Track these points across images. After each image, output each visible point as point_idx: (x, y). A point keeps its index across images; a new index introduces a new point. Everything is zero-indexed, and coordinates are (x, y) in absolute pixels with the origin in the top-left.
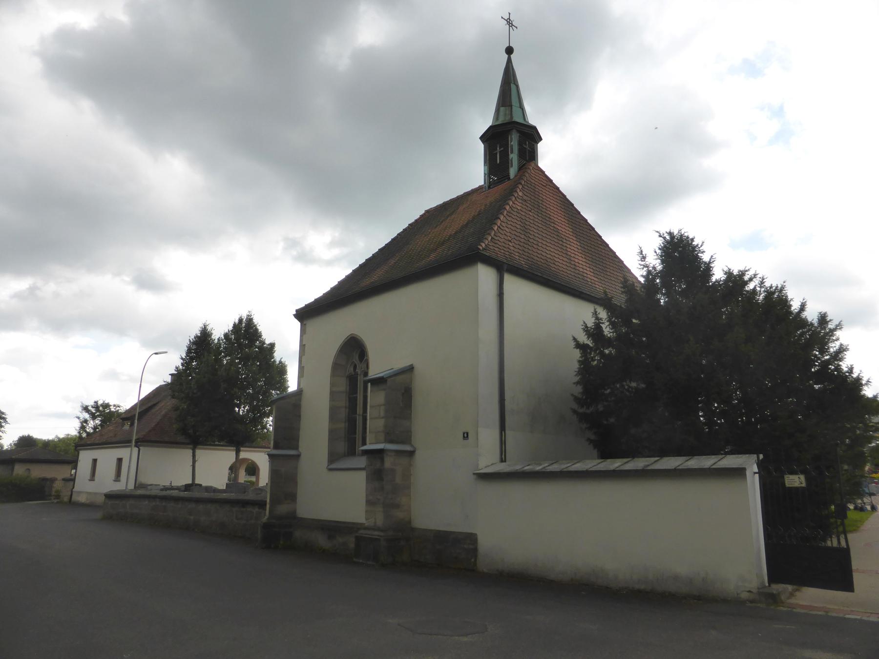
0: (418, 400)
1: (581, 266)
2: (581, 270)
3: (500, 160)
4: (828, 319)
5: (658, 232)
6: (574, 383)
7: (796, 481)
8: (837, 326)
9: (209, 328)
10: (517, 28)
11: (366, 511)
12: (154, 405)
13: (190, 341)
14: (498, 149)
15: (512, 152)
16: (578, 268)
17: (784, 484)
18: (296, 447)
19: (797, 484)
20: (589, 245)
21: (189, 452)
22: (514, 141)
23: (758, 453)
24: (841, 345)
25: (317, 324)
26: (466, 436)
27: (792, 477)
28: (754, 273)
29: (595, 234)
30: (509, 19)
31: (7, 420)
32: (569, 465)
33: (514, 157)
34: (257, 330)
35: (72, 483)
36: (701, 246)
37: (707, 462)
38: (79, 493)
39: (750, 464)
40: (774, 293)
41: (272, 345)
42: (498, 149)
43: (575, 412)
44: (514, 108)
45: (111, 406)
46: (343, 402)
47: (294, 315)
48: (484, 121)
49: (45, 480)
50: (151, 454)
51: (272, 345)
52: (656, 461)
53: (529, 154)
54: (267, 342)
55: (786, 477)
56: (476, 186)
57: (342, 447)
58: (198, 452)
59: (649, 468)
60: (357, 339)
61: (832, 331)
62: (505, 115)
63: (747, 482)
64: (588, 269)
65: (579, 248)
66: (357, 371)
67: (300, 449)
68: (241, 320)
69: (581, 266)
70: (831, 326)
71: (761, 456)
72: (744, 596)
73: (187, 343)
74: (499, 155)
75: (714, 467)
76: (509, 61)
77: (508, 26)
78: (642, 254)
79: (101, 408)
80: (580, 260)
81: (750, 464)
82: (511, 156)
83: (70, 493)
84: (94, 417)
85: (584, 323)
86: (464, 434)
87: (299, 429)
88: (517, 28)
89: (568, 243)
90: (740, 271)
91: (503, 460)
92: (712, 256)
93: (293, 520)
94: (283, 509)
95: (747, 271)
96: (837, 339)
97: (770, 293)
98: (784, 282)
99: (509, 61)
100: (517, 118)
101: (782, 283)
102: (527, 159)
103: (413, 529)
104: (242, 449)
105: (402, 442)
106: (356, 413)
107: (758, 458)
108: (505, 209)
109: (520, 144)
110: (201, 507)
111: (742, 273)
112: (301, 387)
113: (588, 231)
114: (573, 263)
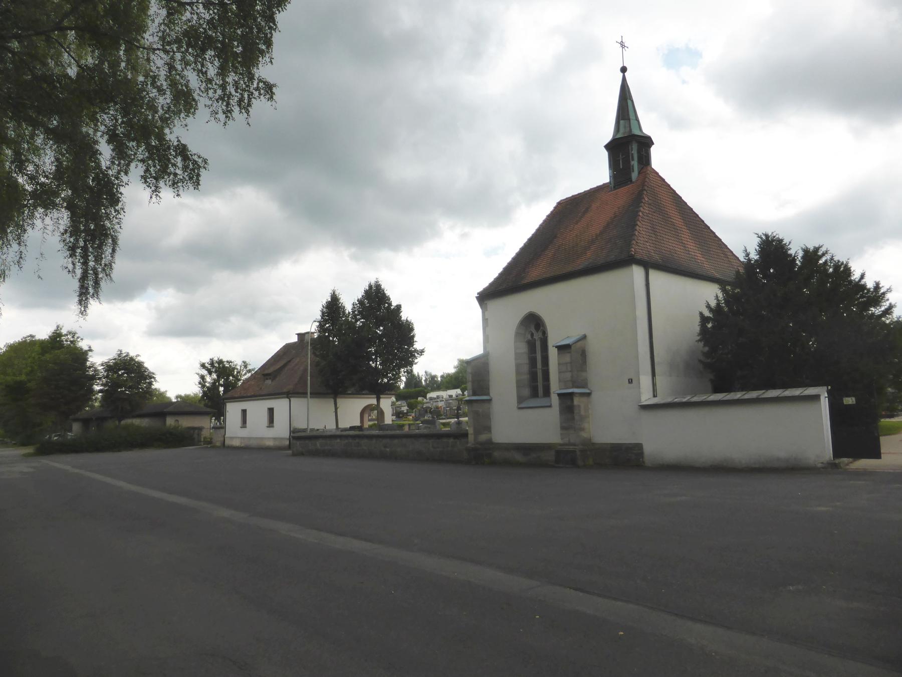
0: (592, 359)
1: (692, 250)
2: (693, 254)
3: (622, 165)
4: (881, 286)
5: (756, 234)
6: (696, 341)
7: (849, 401)
8: (888, 289)
9: (337, 293)
10: (628, 47)
11: (561, 434)
12: (289, 361)
13: (323, 306)
14: (621, 156)
15: (633, 160)
16: (691, 253)
17: (843, 403)
18: (488, 394)
19: (850, 403)
20: (696, 231)
21: (288, 400)
22: (634, 150)
23: (827, 386)
24: (890, 304)
25: (496, 305)
26: (630, 381)
27: (847, 399)
28: (825, 249)
29: (699, 220)
30: (622, 42)
31: (156, 379)
32: (705, 397)
33: (635, 163)
34: (384, 294)
35: (223, 431)
36: (789, 245)
37: (797, 392)
38: (232, 438)
39: (823, 392)
40: (840, 267)
41: (399, 307)
42: (621, 156)
43: (700, 361)
44: (632, 121)
45: (224, 362)
46: (525, 360)
47: (476, 297)
48: (607, 132)
49: (194, 429)
50: (298, 404)
51: (399, 307)
52: (764, 393)
53: (645, 160)
54: (394, 304)
55: (844, 399)
56: (600, 183)
57: (526, 392)
58: (292, 399)
59: (760, 397)
60: (535, 315)
61: (884, 294)
62: (625, 127)
63: (821, 405)
64: (698, 252)
65: (690, 235)
66: (534, 337)
67: (491, 394)
68: (370, 286)
69: (692, 250)
70: (882, 291)
71: (829, 387)
72: (820, 465)
73: (320, 307)
74: (622, 161)
75: (802, 395)
76: (624, 79)
77: (621, 48)
78: (746, 252)
79: (216, 365)
80: (691, 245)
81: (823, 392)
82: (632, 163)
83: (222, 439)
84: (210, 373)
85: (707, 301)
86: (629, 380)
87: (489, 381)
88: (628, 47)
89: (682, 232)
90: (815, 247)
91: (655, 396)
92: (796, 252)
93: (490, 445)
94: (483, 437)
95: (820, 247)
96: (888, 300)
97: (837, 266)
98: (848, 259)
99: (624, 79)
100: (636, 132)
101: (847, 260)
102: (644, 162)
103: (594, 444)
104: (381, 396)
105: (583, 387)
106: (537, 368)
107: (828, 388)
108: (639, 215)
109: (639, 152)
110: (396, 441)
111: (817, 249)
112: (487, 350)
113: (694, 218)
114: (687, 249)
